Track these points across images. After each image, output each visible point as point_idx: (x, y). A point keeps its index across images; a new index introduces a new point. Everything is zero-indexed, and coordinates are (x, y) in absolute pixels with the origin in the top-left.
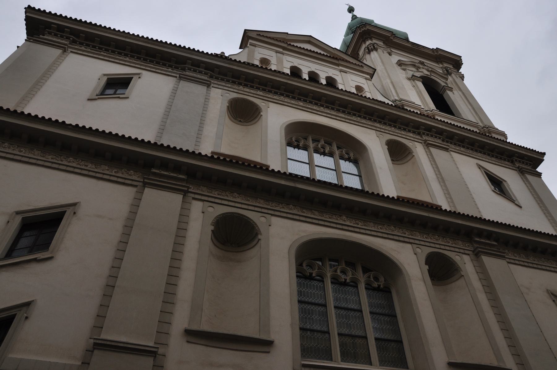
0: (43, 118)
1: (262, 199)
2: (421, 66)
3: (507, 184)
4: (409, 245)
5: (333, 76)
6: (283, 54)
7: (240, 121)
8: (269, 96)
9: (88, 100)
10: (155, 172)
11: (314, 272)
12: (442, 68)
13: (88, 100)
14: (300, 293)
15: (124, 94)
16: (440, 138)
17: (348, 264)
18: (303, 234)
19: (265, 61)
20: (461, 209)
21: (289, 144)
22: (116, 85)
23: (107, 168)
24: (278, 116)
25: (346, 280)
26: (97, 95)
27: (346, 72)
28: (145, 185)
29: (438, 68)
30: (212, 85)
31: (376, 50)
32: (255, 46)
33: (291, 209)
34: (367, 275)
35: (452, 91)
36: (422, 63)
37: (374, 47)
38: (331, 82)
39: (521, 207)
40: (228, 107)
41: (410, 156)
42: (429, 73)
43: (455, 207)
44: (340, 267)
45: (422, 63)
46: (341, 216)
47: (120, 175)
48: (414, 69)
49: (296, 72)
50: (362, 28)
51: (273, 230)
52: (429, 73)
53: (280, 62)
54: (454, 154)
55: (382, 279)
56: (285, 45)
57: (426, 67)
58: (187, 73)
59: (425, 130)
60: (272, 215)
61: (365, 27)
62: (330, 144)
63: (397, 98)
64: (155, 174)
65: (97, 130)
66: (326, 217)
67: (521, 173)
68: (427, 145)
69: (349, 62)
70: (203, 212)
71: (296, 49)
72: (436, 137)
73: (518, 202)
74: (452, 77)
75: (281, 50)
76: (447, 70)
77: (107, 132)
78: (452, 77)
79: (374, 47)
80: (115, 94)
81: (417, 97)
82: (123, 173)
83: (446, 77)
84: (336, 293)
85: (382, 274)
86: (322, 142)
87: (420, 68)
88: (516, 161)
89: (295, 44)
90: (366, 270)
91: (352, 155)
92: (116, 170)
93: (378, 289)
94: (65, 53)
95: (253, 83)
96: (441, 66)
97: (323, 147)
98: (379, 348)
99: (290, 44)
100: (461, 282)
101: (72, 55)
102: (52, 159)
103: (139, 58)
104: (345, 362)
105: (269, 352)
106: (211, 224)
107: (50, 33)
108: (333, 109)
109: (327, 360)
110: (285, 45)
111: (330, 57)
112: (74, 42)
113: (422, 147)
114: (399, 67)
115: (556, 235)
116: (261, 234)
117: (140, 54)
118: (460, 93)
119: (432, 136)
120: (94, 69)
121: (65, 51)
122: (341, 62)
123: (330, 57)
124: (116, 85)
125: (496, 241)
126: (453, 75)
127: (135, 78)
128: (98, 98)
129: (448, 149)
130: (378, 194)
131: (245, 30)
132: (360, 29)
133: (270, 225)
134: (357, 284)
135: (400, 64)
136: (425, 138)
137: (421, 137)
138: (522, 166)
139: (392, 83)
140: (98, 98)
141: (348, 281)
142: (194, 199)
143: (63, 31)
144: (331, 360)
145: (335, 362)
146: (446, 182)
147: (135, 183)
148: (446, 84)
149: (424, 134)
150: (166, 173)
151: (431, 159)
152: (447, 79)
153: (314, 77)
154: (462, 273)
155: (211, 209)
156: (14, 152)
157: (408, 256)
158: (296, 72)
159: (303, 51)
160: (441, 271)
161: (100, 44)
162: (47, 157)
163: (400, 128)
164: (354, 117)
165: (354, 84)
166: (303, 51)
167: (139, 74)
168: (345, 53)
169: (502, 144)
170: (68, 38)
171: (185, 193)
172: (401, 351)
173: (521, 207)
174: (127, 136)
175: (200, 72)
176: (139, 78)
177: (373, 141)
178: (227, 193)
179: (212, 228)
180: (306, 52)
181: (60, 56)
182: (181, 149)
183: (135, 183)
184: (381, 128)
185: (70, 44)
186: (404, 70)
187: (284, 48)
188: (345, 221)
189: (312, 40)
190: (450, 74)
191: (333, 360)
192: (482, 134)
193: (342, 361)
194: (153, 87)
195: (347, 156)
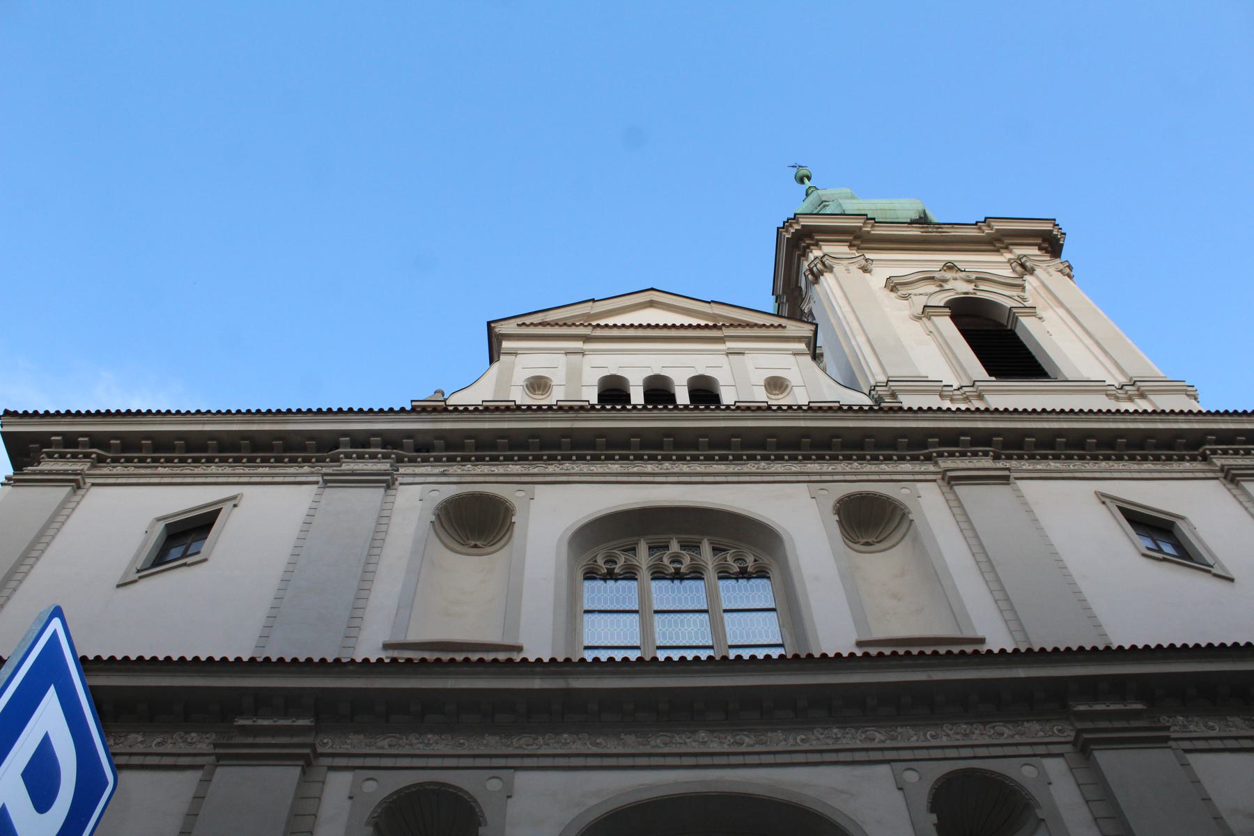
0: (168, 659)
1: (630, 733)
2: (948, 275)
5: (708, 373)
6: (583, 353)
7: (476, 546)
8: (536, 471)
9: (118, 586)
10: (243, 726)
12: (1009, 261)
13: (118, 586)
15: (198, 553)
16: (986, 454)
18: (592, 802)
20: (1044, 639)
22: (185, 536)
23: (140, 738)
24: (554, 509)
26: (138, 571)
27: (740, 353)
29: (997, 264)
30: (400, 480)
31: (830, 269)
33: (566, 744)
35: (1034, 315)
37: (823, 264)
38: (704, 393)
41: (904, 526)
42: (969, 288)
43: (1027, 639)
45: (950, 267)
46: (694, 732)
47: (169, 748)
48: (932, 288)
49: (613, 392)
50: (791, 226)
51: (515, 808)
52: (969, 288)
53: (574, 375)
54: (1030, 489)
58: (344, 467)
59: (941, 444)
60: (516, 768)
61: (797, 223)
62: (694, 547)
64: (244, 730)
65: (210, 659)
66: (658, 743)
68: (951, 481)
69: (756, 325)
70: (351, 798)
71: (615, 332)
72: (975, 454)
74: (1038, 278)
75: (578, 345)
76: (1022, 265)
78: (1038, 278)
79: (823, 264)
80: (184, 555)
81: (936, 363)
82: (411, 745)
83: (1019, 282)
87: (946, 281)
89: (611, 322)
92: (158, 740)
94: (81, 492)
96: (1008, 256)
97: (676, 559)
99: (598, 325)
101: (95, 490)
102: (390, 746)
103: (237, 460)
106: (367, 824)
107: (50, 456)
108: (695, 459)
111: (715, 326)
112: (101, 460)
113: (938, 491)
114: (893, 295)
115: (1248, 644)
116: (1040, 807)
117: (239, 451)
118: (1061, 311)
119: (963, 454)
120: (129, 510)
121: (79, 487)
123: (715, 326)
124: (185, 536)
126: (1038, 271)
127: (226, 507)
128: (140, 578)
129: (1007, 478)
130: (810, 656)
131: (489, 323)
132: (787, 231)
133: (509, 797)
135: (893, 285)
137: (936, 463)
140: (140, 578)
142: (332, 768)
143: (75, 444)
146: (998, 569)
147: (199, 761)
148: (1024, 299)
149: (940, 455)
150: (266, 723)
151: (960, 518)
152: (1023, 288)
153: (659, 392)
155: (370, 787)
156: (583, 750)
158: (613, 392)
159: (631, 332)
161: (154, 452)
162: (653, 743)
163: (875, 458)
164: (751, 463)
165: (760, 377)
166: (631, 332)
167: (234, 498)
168: (778, 315)
169: (1162, 421)
170: (87, 456)
171: (308, 762)
175: (373, 456)
176: (235, 506)
177: (795, 507)
180: (640, 333)
181: (66, 501)
183: (199, 761)
184: (821, 474)
185: (93, 466)
186: (905, 297)
187: (587, 339)
188: (704, 743)
189: (655, 298)
190: (1031, 271)
194: (267, 515)
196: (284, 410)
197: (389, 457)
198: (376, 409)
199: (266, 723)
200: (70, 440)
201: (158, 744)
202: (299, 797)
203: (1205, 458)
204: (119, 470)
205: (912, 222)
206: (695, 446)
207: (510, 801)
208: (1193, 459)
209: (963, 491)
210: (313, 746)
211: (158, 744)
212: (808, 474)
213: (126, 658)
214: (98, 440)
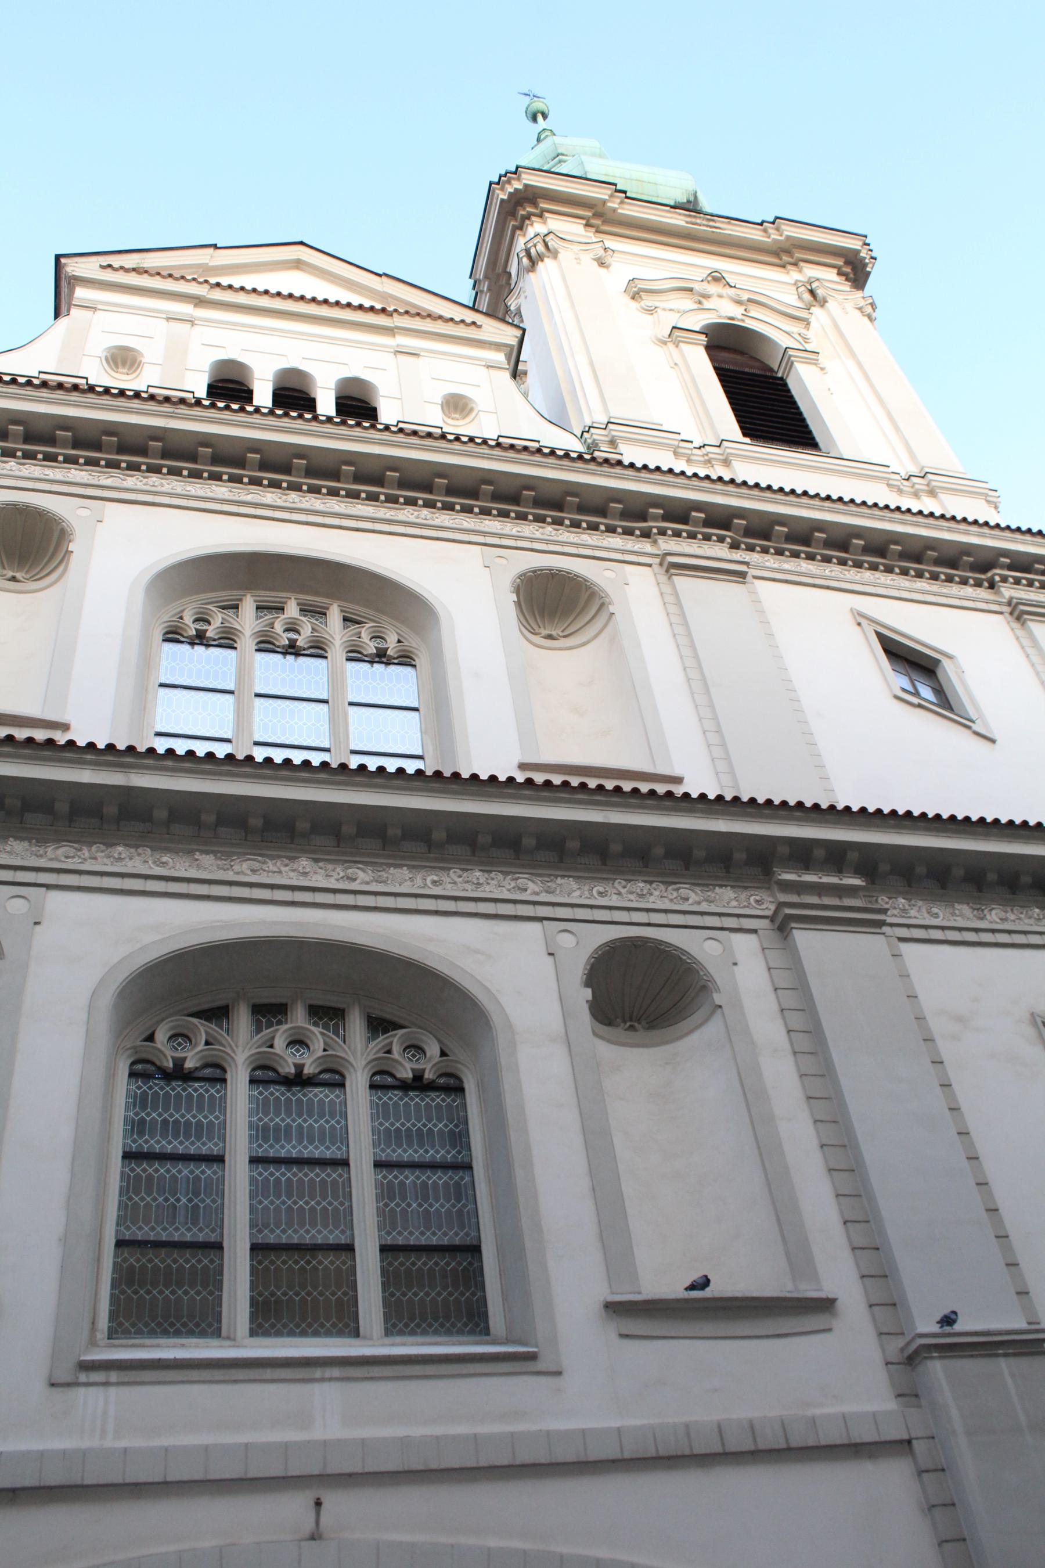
3: (958, 666)
4: (536, 926)
11: (190, 1054)
14: (136, 1127)
16: (721, 539)
17: (320, 1013)
19: (123, 358)
21: (173, 635)
24: (131, 539)
25: (299, 1068)
28: (783, 925)
29: (779, 285)
32: (94, 309)
34: (381, 1040)
35: (815, 363)
36: (717, 278)
39: (993, 741)
40: (518, 604)
44: (285, 1027)
45: (717, 278)
52: (737, 312)
55: (433, 1050)
56: (202, 291)
57: (731, 292)
59: (665, 518)
60: (48, 887)
61: (519, 179)
62: (321, 613)
63: (914, 470)
67: (1018, 619)
72: (707, 538)
73: (986, 724)
76: (812, 292)
77: (974, 818)
84: (266, 1114)
85: (425, 1032)
86: (292, 610)
87: (707, 296)
88: (1004, 579)
89: (237, 281)
90: (378, 1026)
91: (391, 645)
93: (418, 1084)
95: (644, 519)
97: (292, 628)
98: (389, 1279)
99: (218, 285)
100: (713, 1029)
104: (266, 1334)
105: (829, 1330)
109: (340, 1333)
110: (202, 291)
119: (692, 536)
122: (398, 321)
125: (858, 872)
126: (831, 304)
129: (742, 575)
134: (343, 1076)
136: (1008, 591)
138: (1022, 593)
139: (592, 364)
141: (189, 1064)
144: (356, 1334)
145: (228, 1338)
148: (806, 340)
149: (662, 532)
154: (718, 998)
157: (516, 962)
160: (640, 993)
162: (237, 868)
165: (438, 393)
172: (474, 1278)
173: (993, 741)
174: (945, 816)
177: (460, 576)
178: (94, 848)
179: (588, 993)
182: (953, 818)
186: (650, 311)
187: (200, 302)
188: (305, 874)
191: (224, 1333)
192: (580, 457)
193: (253, 1333)
195: (371, 648)
208: (978, 584)
212: (485, 534)
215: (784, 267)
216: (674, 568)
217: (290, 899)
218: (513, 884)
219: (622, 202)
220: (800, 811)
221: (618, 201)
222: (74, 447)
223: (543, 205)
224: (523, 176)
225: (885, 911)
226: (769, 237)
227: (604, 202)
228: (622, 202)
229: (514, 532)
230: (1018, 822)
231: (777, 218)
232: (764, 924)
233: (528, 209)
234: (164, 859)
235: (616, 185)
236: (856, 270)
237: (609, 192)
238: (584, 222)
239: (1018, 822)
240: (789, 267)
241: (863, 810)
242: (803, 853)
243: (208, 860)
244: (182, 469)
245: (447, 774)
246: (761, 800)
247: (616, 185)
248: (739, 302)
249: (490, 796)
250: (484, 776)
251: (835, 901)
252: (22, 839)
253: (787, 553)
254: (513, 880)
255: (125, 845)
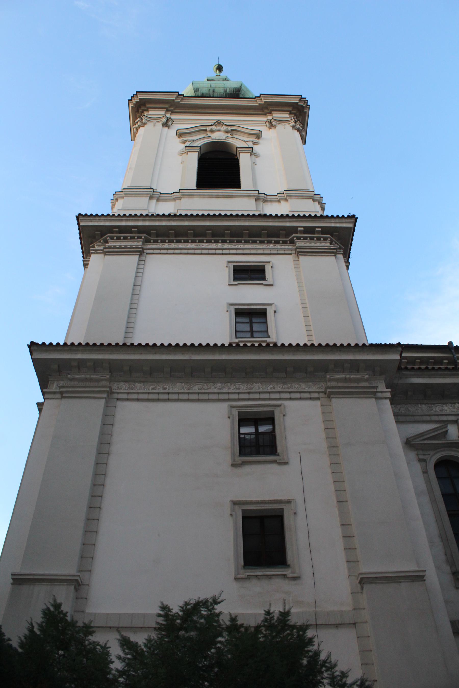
92: (153, 387)
133: (284, 415)
196: (94, 214)
197: (141, 238)
198: (105, 214)
199: (83, 376)
200: (309, 230)
201: (153, 389)
202: (105, 415)
203: (292, 242)
204: (271, 246)
205: (212, 125)
206: (187, 235)
207: (285, 417)
208: (285, 242)
209: (303, 259)
210: (110, 387)
211: (153, 389)
212: (188, 249)
213: (44, 344)
214: (142, 230)
215: (266, 115)
216: (300, 252)
217: (217, 398)
218: (235, 387)
219: (182, 99)
220: (342, 348)
221: (181, 99)
222: (194, 237)
223: (148, 106)
224: (138, 96)
225: (376, 387)
226: (257, 103)
227: (297, 103)
228: (182, 99)
229: (214, 247)
230: (204, 344)
231: (260, 95)
232: (322, 395)
233: (265, 111)
234: (165, 387)
235: (178, 92)
236: (298, 111)
237: (175, 96)
238: (289, 113)
239: (204, 344)
240: (267, 114)
241: (327, 345)
242: (339, 366)
243: (303, 385)
244: (257, 240)
245: (360, 345)
246: (113, 344)
247: (178, 92)
248: (227, 132)
249: (314, 354)
250: (324, 344)
251: (356, 385)
252: (243, 382)
253: (322, 239)
254: (235, 385)
255: (221, 382)
